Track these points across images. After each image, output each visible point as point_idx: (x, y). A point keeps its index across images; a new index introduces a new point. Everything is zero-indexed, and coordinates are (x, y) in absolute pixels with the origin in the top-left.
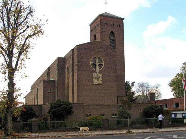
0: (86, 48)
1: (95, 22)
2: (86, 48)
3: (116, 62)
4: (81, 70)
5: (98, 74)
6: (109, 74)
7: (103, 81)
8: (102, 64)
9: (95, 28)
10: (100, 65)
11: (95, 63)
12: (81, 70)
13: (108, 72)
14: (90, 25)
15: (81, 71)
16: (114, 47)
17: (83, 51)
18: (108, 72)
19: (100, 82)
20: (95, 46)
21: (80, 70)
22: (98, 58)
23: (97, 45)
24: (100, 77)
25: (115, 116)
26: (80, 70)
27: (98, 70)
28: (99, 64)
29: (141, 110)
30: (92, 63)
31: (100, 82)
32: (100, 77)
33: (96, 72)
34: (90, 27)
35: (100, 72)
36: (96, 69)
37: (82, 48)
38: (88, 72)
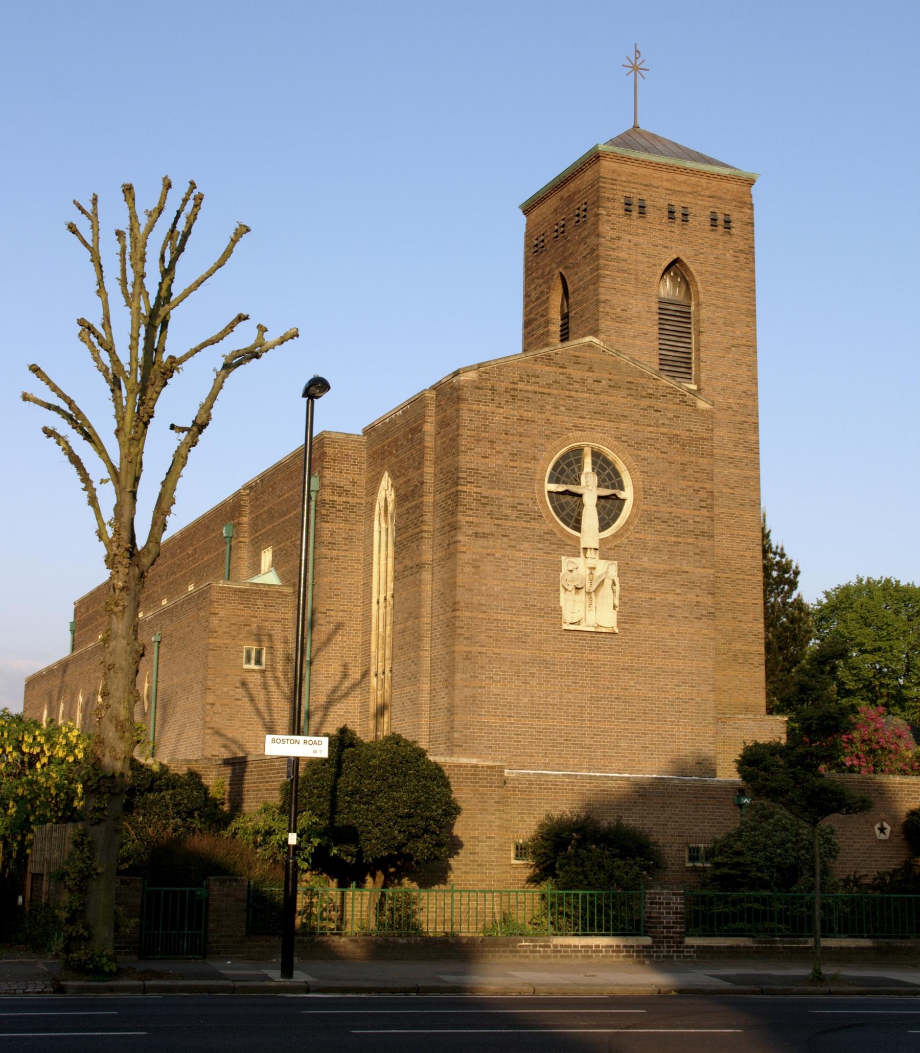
0: (520, 386)
1: (564, 193)
2: (520, 386)
3: (708, 485)
4: (484, 536)
5: (593, 559)
6: (662, 567)
7: (627, 612)
8: (622, 495)
9: (561, 232)
10: (609, 507)
11: (573, 488)
12: (484, 536)
13: (656, 550)
14: (528, 209)
15: (482, 542)
16: (679, 363)
17: (499, 406)
18: (656, 550)
19: (602, 615)
20: (576, 373)
21: (476, 534)
22: (597, 456)
23: (590, 370)
24: (608, 583)
25: (823, 922)
26: (476, 534)
27: (590, 530)
28: (599, 497)
29: (882, 830)
30: (553, 487)
31: (602, 615)
32: (608, 583)
33: (576, 550)
34: (523, 219)
35: (605, 551)
36: (578, 529)
37: (493, 389)
38: (526, 545)
